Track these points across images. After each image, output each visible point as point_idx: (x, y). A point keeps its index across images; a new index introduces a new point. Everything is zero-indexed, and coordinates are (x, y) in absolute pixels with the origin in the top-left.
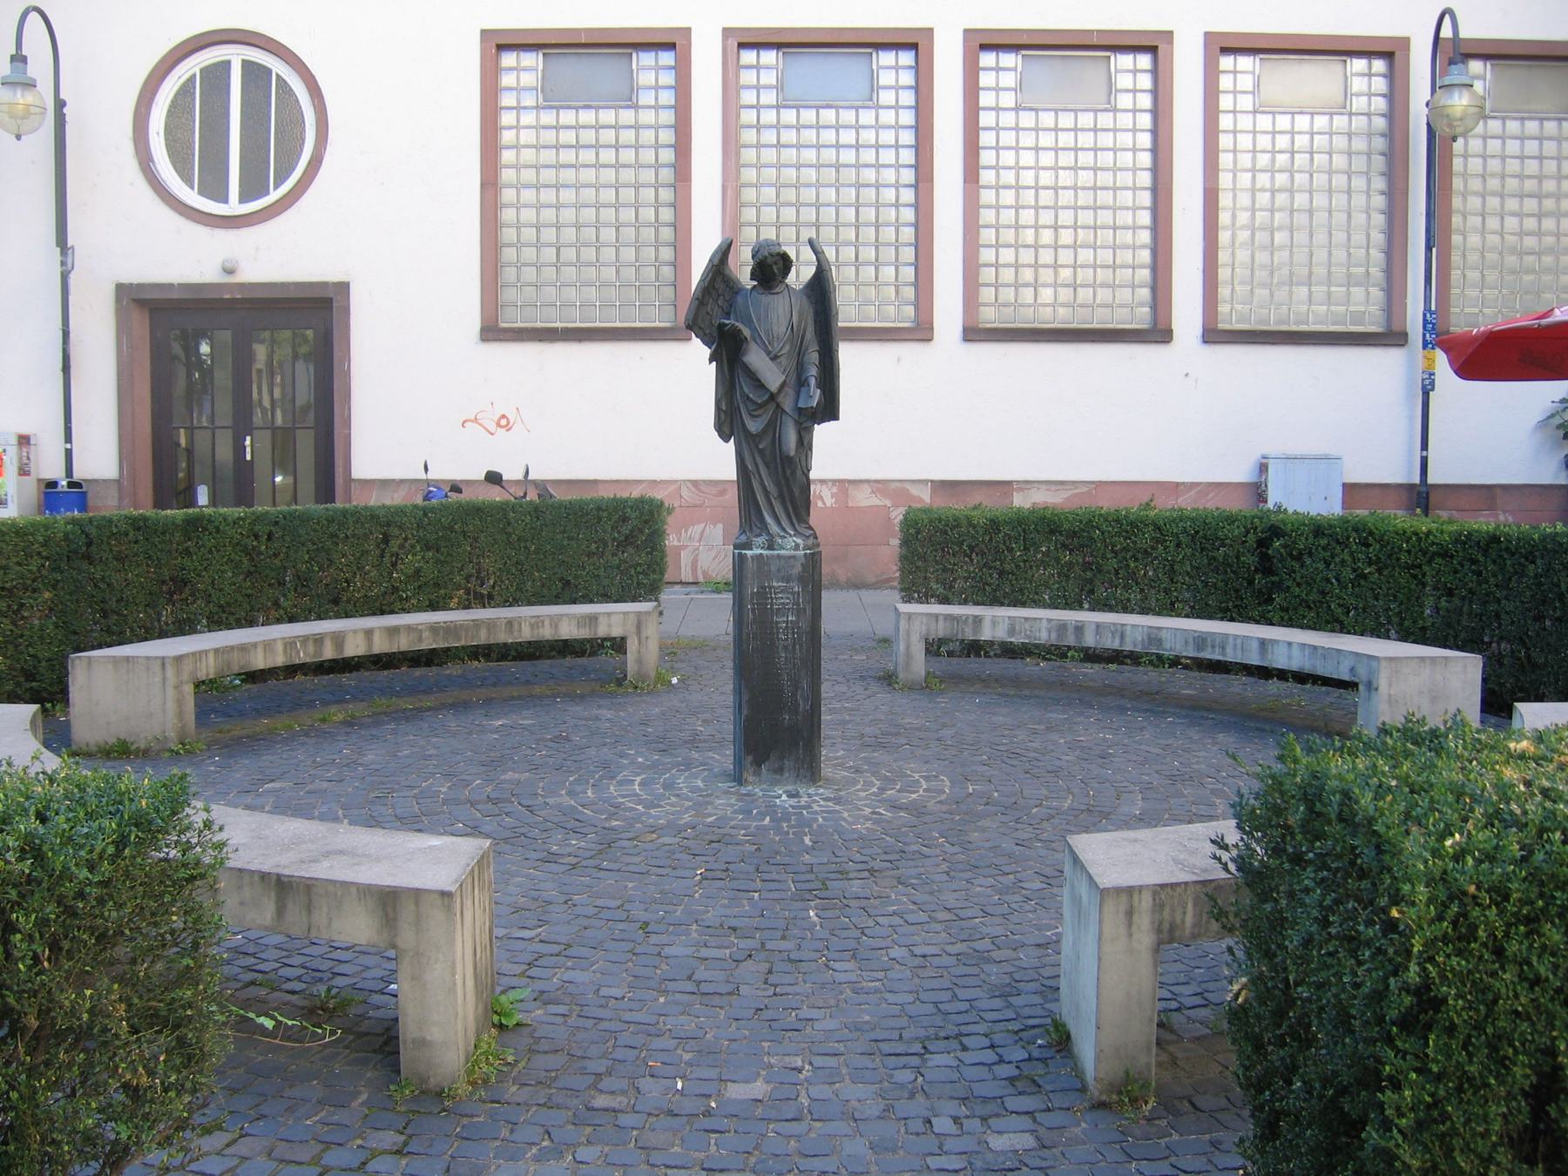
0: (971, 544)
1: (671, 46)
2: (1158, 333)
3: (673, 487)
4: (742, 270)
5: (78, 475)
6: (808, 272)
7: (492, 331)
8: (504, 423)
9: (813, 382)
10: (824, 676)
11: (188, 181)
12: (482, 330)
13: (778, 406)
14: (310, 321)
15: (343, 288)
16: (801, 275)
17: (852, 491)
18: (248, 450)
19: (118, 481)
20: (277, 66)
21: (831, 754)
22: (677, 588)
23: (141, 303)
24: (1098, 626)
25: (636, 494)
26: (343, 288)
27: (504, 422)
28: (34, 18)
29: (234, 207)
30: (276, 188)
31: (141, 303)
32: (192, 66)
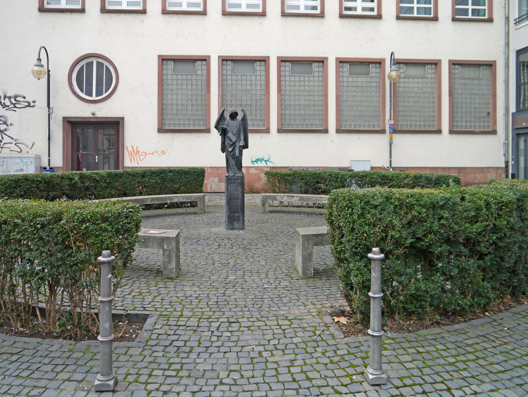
1: (205, 60)
2: (326, 131)
5: (51, 166)
7: (161, 130)
8: (163, 153)
10: (225, 209)
15: (123, 119)
16: (239, 117)
17: (250, 169)
19: (62, 168)
20: (106, 63)
23: (68, 122)
26: (123, 119)
28: (43, 49)
29: (94, 98)
30: (105, 93)
31: (68, 122)
32: (84, 63)
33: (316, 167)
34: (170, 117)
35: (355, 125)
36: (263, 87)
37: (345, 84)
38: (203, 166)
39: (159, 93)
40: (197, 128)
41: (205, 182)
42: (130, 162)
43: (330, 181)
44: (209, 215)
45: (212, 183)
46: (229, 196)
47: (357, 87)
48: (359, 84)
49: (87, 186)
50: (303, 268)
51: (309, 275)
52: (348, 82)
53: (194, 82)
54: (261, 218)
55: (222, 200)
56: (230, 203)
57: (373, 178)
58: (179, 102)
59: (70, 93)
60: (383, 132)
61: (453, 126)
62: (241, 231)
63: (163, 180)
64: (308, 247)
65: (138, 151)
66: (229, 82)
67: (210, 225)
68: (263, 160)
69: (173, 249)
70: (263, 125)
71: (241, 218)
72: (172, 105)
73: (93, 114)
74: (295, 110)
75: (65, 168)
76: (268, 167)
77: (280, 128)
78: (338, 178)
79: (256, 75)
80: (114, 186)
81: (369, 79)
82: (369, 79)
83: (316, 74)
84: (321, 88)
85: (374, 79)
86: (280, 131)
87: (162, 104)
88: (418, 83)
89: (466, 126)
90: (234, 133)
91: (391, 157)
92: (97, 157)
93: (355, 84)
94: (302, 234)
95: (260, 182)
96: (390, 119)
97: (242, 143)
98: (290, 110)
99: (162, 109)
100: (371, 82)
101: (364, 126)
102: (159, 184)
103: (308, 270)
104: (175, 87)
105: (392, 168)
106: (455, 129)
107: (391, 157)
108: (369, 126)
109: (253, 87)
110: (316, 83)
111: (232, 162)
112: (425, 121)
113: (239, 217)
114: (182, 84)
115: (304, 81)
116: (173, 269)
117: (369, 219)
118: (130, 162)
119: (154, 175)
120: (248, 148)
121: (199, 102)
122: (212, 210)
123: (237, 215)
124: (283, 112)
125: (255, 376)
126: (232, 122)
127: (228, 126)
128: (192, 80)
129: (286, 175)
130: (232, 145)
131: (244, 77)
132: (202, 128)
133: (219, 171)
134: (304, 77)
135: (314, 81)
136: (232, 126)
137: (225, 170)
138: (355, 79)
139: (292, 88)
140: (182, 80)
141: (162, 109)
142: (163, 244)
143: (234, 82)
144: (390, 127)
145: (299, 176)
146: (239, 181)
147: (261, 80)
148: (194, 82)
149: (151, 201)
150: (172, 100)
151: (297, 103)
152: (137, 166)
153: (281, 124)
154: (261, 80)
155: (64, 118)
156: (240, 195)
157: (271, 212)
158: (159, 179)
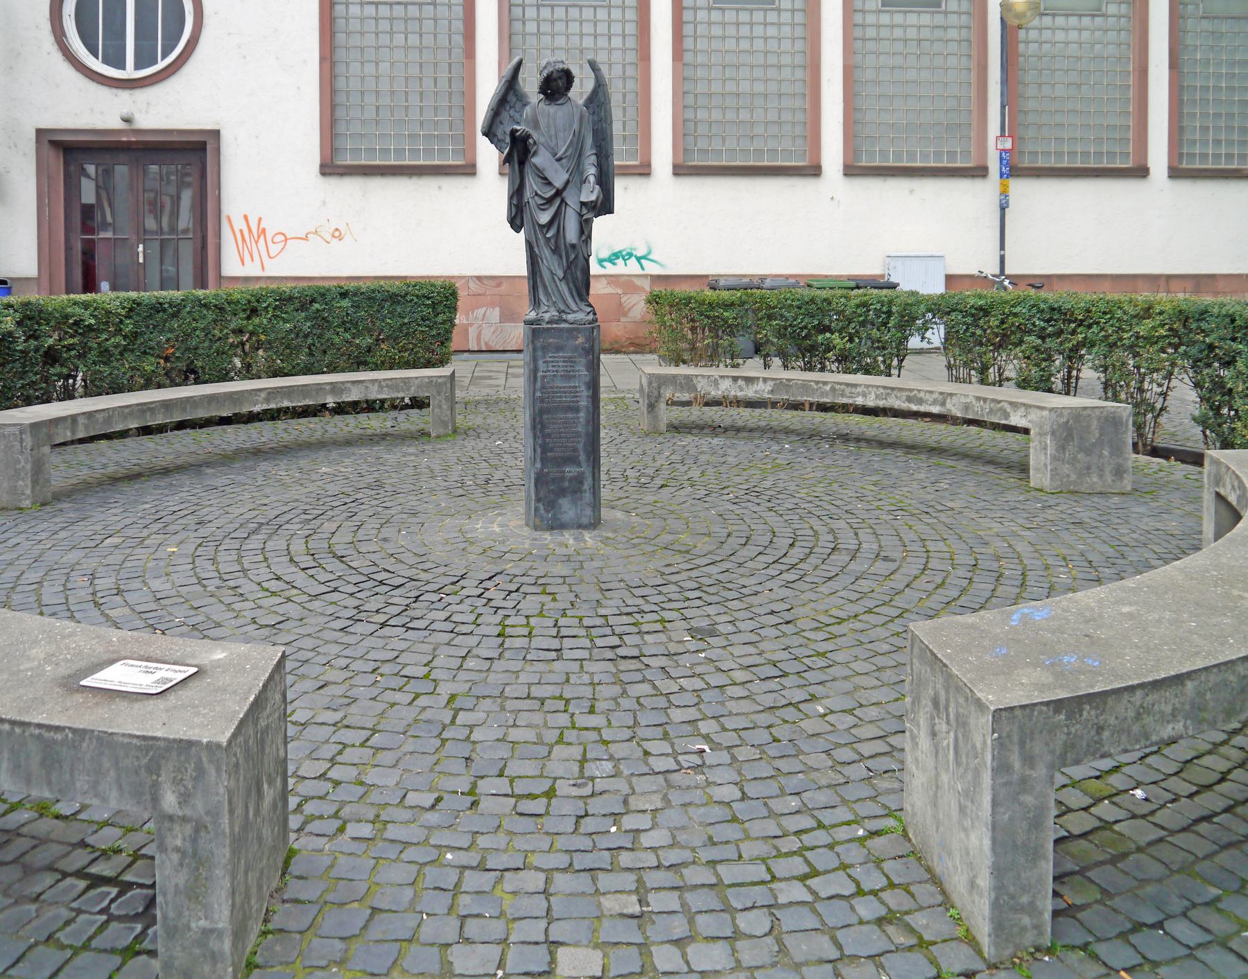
0: (712, 316)
2: (815, 171)
4: (530, 84)
6: (590, 85)
7: (329, 169)
8: (337, 234)
9: (592, 179)
11: (95, 53)
12: (322, 166)
13: (563, 201)
14: (191, 157)
15: (216, 134)
16: (580, 90)
18: (141, 256)
19: (37, 279)
21: (33, 135)
22: (466, 355)
23: (55, 144)
24: (71, 397)
26: (216, 134)
27: (337, 234)
29: (130, 72)
30: (163, 58)
31: (55, 144)
33: (787, 277)
34: (356, 128)
35: (898, 155)
36: (631, 43)
37: (871, 33)
38: (455, 272)
39: (322, 59)
41: (459, 319)
42: (239, 263)
43: (863, 324)
44: (470, 443)
45: (476, 324)
46: (542, 401)
47: (906, 41)
48: (912, 33)
49: (50, 347)
50: (996, 905)
51: (1029, 939)
52: (878, 26)
53: (428, 25)
54: (648, 459)
55: (512, 382)
56: (543, 427)
57: (1015, 315)
58: (384, 86)
59: (57, 56)
60: (980, 172)
61: (1181, 155)
62: (587, 535)
63: (321, 321)
64: (1024, 780)
65: (264, 230)
66: (531, 27)
67: (463, 511)
68: (630, 255)
69: (214, 814)
70: (632, 154)
71: (587, 485)
72: (362, 93)
73: (127, 120)
74: (724, 109)
75: (45, 282)
76: (646, 276)
77: (680, 161)
78: (889, 313)
80: (152, 344)
81: (939, 19)
82: (939, 19)
84: (799, 45)
85: (953, 19)
86: (680, 170)
87: (333, 91)
88: (1080, 30)
89: (1217, 157)
90: (558, 150)
91: (1002, 247)
92: (141, 248)
93: (898, 33)
94: (993, 698)
95: (623, 319)
96: (1003, 135)
97: (590, 193)
98: (710, 109)
99: (333, 107)
100: (946, 28)
101: (925, 156)
102: (306, 336)
103: (1022, 909)
104: (370, 40)
105: (1008, 277)
106: (1184, 165)
107: (1002, 247)
108: (938, 155)
109: (602, 42)
110: (786, 30)
111: (552, 265)
112: (1099, 141)
113: (579, 480)
114: (391, 33)
115: (752, 24)
116: (220, 934)
117: (1068, 476)
118: (239, 263)
119: (290, 308)
120: (611, 211)
121: (443, 85)
122: (478, 421)
123: (570, 471)
124: (689, 114)
125: (590, 812)
126: (552, 109)
127: (536, 125)
128: (420, 20)
129: (718, 305)
130: (550, 201)
131: (574, 13)
132: (451, 162)
134: (751, 11)
136: (553, 126)
137: (525, 288)
138: (898, 19)
139: (716, 45)
140: (391, 19)
141: (333, 107)
142: (156, 786)
143: (545, 27)
144: (1001, 159)
145: (760, 309)
146: (580, 340)
147: (624, 22)
148: (428, 25)
149: (267, 400)
150: (362, 79)
151: (731, 87)
152: (260, 274)
153: (685, 150)
154: (624, 22)
155: (40, 132)
156: (584, 393)
157: (675, 428)
158: (307, 319)
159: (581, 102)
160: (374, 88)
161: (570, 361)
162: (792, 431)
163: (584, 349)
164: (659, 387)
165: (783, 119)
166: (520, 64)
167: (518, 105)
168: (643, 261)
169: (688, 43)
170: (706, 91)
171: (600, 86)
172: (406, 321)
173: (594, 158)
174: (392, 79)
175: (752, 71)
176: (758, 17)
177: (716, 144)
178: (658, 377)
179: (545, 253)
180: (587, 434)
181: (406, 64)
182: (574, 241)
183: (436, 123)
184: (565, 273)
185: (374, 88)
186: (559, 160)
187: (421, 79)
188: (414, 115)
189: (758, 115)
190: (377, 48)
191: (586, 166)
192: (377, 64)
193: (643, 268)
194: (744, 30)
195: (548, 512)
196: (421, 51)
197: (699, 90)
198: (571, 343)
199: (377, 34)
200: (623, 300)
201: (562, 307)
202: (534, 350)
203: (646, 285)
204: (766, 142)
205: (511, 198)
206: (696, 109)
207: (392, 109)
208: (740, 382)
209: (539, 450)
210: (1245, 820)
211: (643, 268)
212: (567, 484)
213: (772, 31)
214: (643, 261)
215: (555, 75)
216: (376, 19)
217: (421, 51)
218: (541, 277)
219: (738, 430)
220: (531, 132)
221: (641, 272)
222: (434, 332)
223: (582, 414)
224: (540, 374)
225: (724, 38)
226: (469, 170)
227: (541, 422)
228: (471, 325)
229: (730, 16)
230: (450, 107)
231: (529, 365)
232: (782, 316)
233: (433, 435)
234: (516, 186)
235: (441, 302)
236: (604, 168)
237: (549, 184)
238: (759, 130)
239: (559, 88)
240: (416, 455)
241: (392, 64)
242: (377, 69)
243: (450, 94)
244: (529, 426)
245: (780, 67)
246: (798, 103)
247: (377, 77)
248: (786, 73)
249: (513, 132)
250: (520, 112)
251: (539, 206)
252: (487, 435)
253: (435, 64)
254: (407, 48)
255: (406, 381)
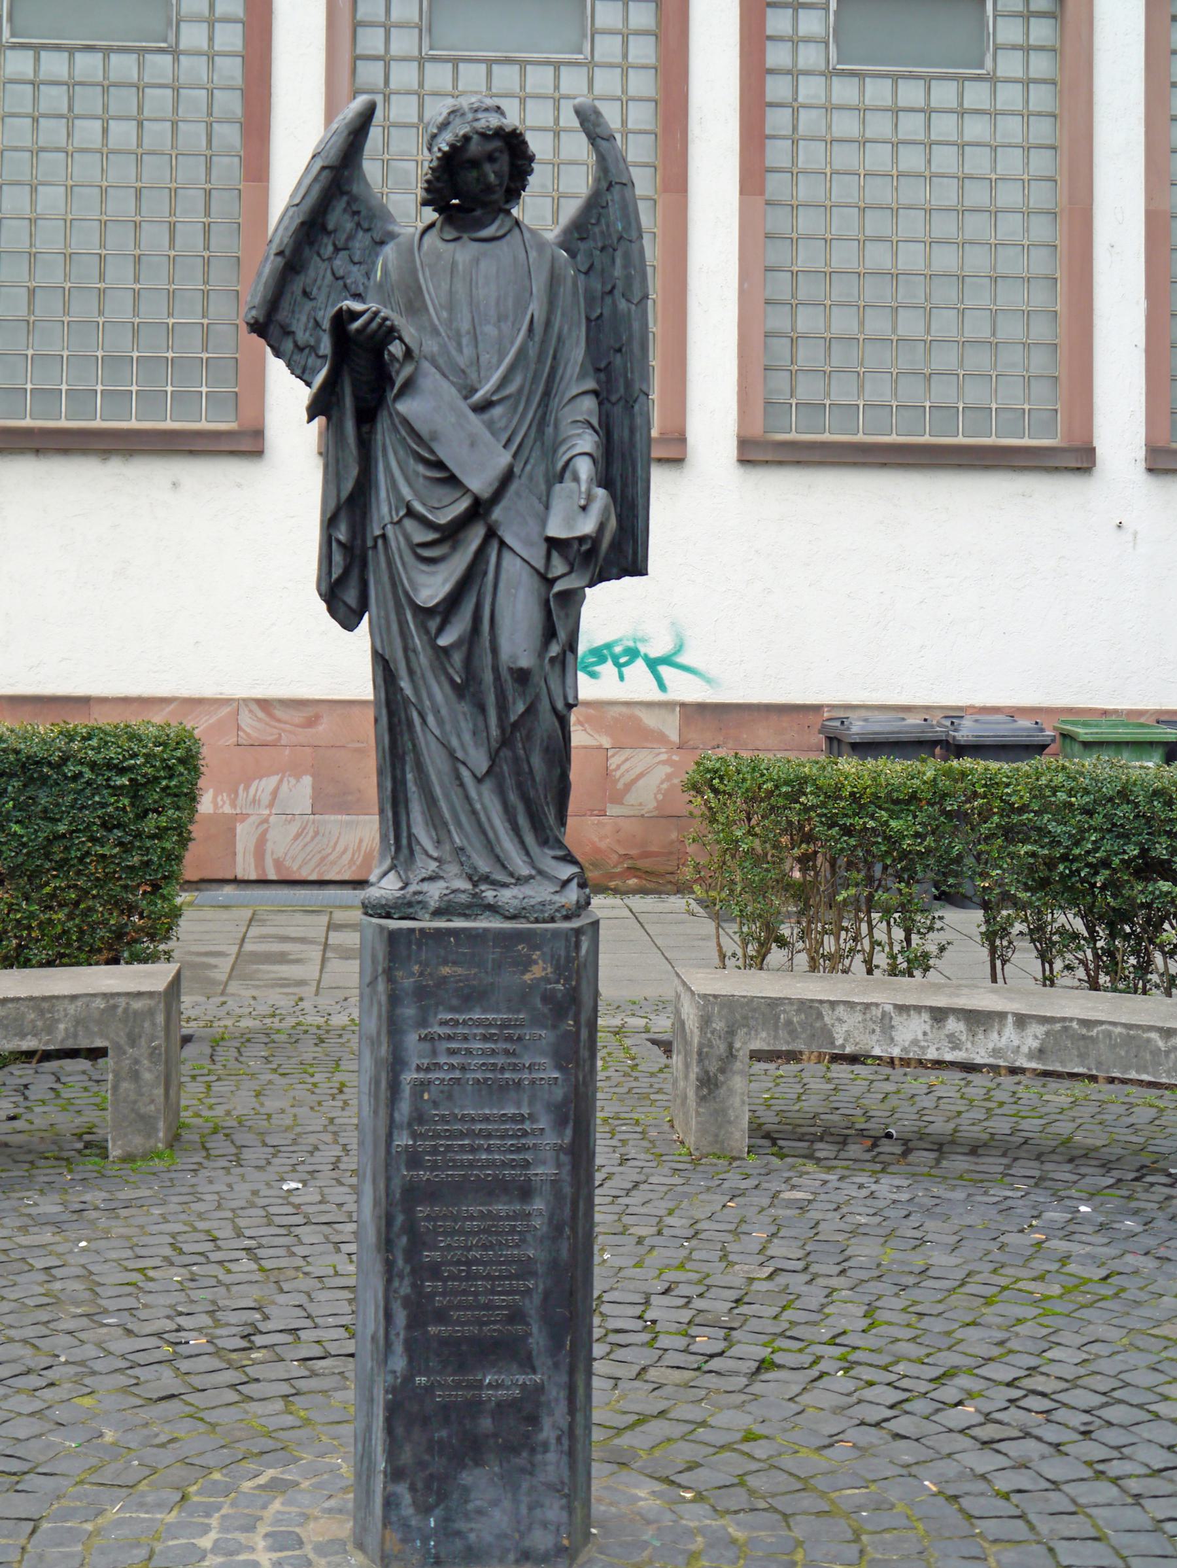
2: (1077, 459)
3: (225, 711)
4: (398, 179)
6: (579, 183)
9: (584, 468)
13: (491, 533)
16: (546, 206)
22: (228, 890)
25: (158, 718)
40: (169, 425)
45: (252, 816)
46: (414, 1159)
56: (417, 1242)
58: (50, 240)
68: (633, 654)
74: (862, 310)
76: (668, 705)
77: (756, 430)
79: (591, 65)
83: (1010, 65)
86: (755, 452)
97: (578, 513)
98: (827, 309)
110: (1011, 128)
111: (452, 733)
113: (526, 1410)
114: (70, 117)
115: (928, 111)
120: (637, 568)
121: (190, 239)
123: (500, 1382)
126: (464, 252)
127: (414, 305)
128: (139, 88)
130: (451, 534)
133: (324, 729)
135: (993, 114)
136: (459, 302)
137: (366, 732)
139: (845, 157)
140: (71, 85)
146: (538, 971)
151: (877, 256)
156: (549, 1138)
159: (552, 234)
160: (24, 245)
161: (507, 1036)
162: (1087, 1154)
163: (547, 998)
164: (731, 1033)
165: (1001, 335)
166: (366, 118)
167: (361, 241)
168: (664, 670)
169: (777, 153)
170: (820, 265)
171: (610, 182)
172: (62, 828)
173: (589, 404)
174: (68, 224)
175: (928, 221)
176: (944, 93)
177: (842, 392)
178: (729, 1003)
179: (435, 695)
180: (554, 1265)
181: (104, 191)
182: (524, 662)
183: (170, 330)
184: (494, 758)
185: (24, 245)
186: (482, 408)
187: (137, 226)
188: (120, 310)
189: (944, 324)
190: (36, 152)
191: (567, 430)
192: (34, 190)
193: (662, 686)
194: (912, 125)
195: (427, 1510)
196: (139, 161)
197: (801, 265)
198: (509, 979)
199: (35, 120)
200: (614, 762)
201: (484, 866)
202: (394, 999)
203: (671, 727)
204: (960, 389)
205: (330, 523)
206: (794, 308)
207: (67, 296)
208: (953, 1025)
209: (401, 1317)
210: (1133, 1170)
211: (662, 686)
212: (486, 1424)
213: (976, 129)
214: (664, 670)
215: (475, 148)
216: (35, 84)
217: (139, 161)
218: (420, 767)
219: (941, 1147)
220: (398, 320)
221: (656, 695)
222: (135, 860)
223: (538, 1205)
224: (409, 1077)
225: (863, 142)
226: (248, 443)
227: (411, 1228)
228: (243, 817)
229: (878, 92)
230: (206, 294)
231: (374, 1043)
232: (1042, 831)
233: (115, 1152)
234: (348, 486)
235: (156, 779)
236: (620, 433)
237: (452, 480)
238: (945, 359)
239: (489, 189)
240: (58, 1225)
241: (70, 190)
242: (33, 203)
243: (207, 262)
244: (371, 1236)
245: (995, 213)
246: (1039, 298)
247: (33, 221)
248: (1010, 226)
249: (342, 319)
250: (366, 264)
251: (414, 547)
252: (261, 1153)
253: (174, 193)
254: (105, 153)
255: (44, 1004)
